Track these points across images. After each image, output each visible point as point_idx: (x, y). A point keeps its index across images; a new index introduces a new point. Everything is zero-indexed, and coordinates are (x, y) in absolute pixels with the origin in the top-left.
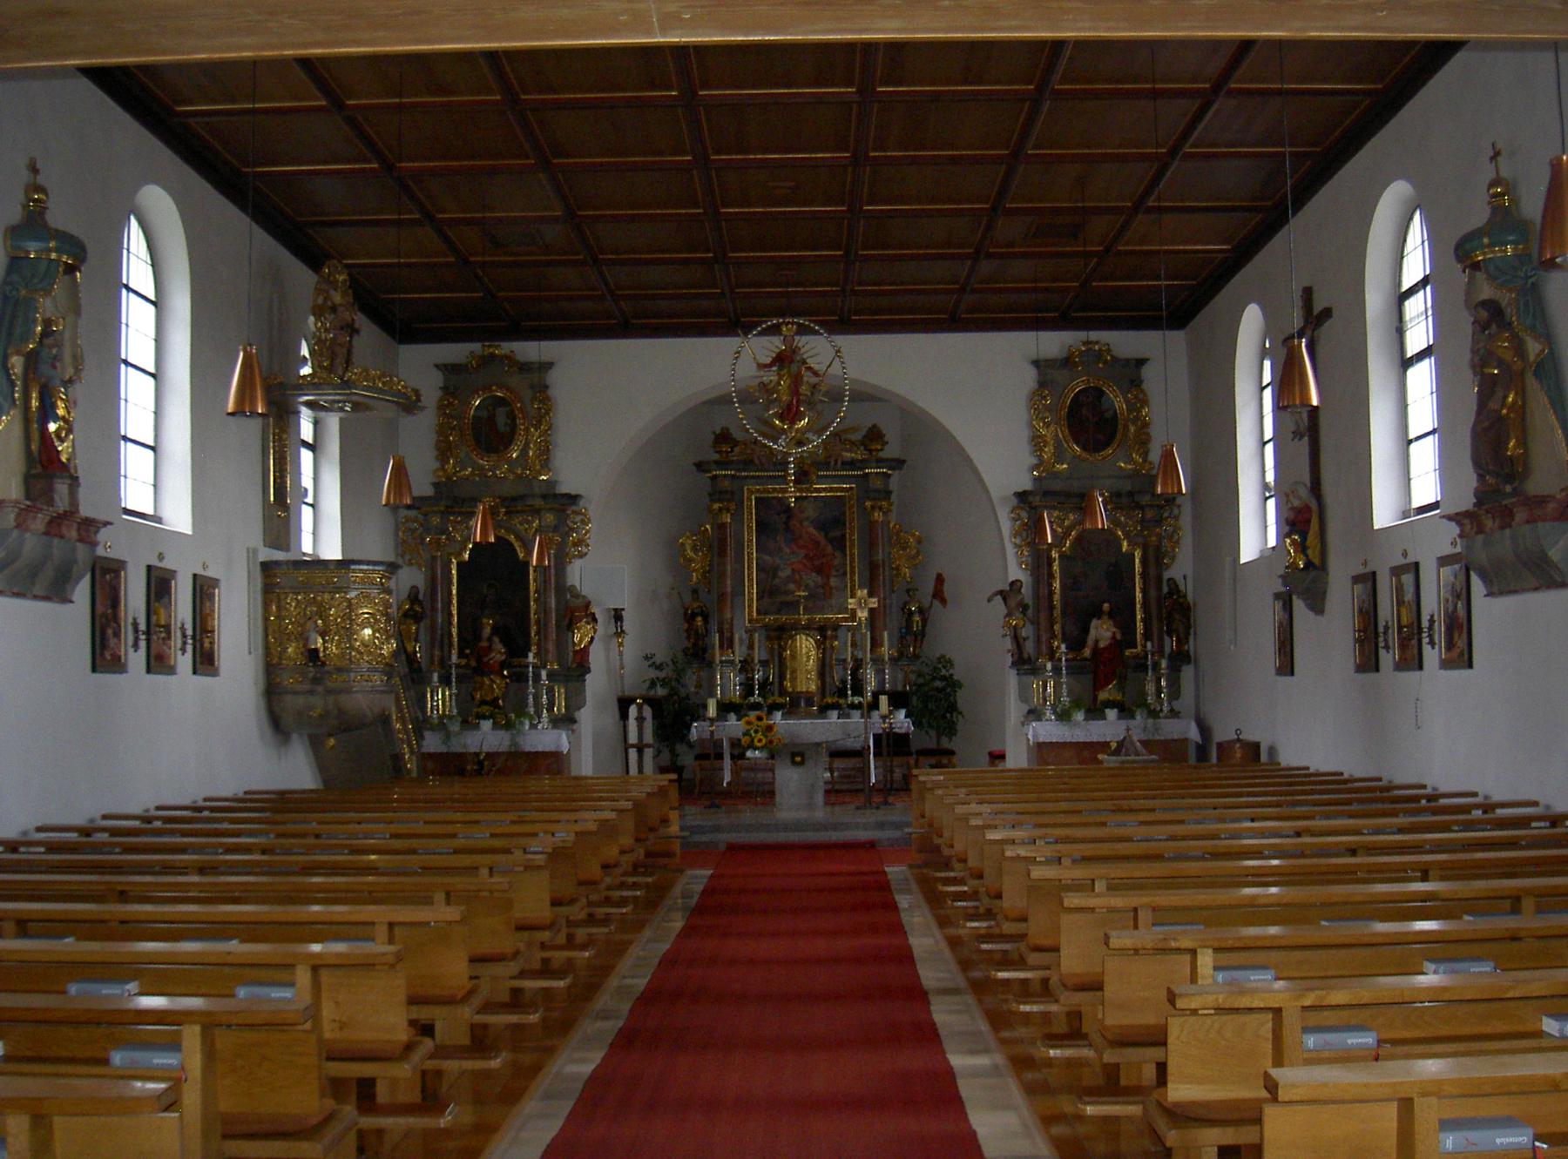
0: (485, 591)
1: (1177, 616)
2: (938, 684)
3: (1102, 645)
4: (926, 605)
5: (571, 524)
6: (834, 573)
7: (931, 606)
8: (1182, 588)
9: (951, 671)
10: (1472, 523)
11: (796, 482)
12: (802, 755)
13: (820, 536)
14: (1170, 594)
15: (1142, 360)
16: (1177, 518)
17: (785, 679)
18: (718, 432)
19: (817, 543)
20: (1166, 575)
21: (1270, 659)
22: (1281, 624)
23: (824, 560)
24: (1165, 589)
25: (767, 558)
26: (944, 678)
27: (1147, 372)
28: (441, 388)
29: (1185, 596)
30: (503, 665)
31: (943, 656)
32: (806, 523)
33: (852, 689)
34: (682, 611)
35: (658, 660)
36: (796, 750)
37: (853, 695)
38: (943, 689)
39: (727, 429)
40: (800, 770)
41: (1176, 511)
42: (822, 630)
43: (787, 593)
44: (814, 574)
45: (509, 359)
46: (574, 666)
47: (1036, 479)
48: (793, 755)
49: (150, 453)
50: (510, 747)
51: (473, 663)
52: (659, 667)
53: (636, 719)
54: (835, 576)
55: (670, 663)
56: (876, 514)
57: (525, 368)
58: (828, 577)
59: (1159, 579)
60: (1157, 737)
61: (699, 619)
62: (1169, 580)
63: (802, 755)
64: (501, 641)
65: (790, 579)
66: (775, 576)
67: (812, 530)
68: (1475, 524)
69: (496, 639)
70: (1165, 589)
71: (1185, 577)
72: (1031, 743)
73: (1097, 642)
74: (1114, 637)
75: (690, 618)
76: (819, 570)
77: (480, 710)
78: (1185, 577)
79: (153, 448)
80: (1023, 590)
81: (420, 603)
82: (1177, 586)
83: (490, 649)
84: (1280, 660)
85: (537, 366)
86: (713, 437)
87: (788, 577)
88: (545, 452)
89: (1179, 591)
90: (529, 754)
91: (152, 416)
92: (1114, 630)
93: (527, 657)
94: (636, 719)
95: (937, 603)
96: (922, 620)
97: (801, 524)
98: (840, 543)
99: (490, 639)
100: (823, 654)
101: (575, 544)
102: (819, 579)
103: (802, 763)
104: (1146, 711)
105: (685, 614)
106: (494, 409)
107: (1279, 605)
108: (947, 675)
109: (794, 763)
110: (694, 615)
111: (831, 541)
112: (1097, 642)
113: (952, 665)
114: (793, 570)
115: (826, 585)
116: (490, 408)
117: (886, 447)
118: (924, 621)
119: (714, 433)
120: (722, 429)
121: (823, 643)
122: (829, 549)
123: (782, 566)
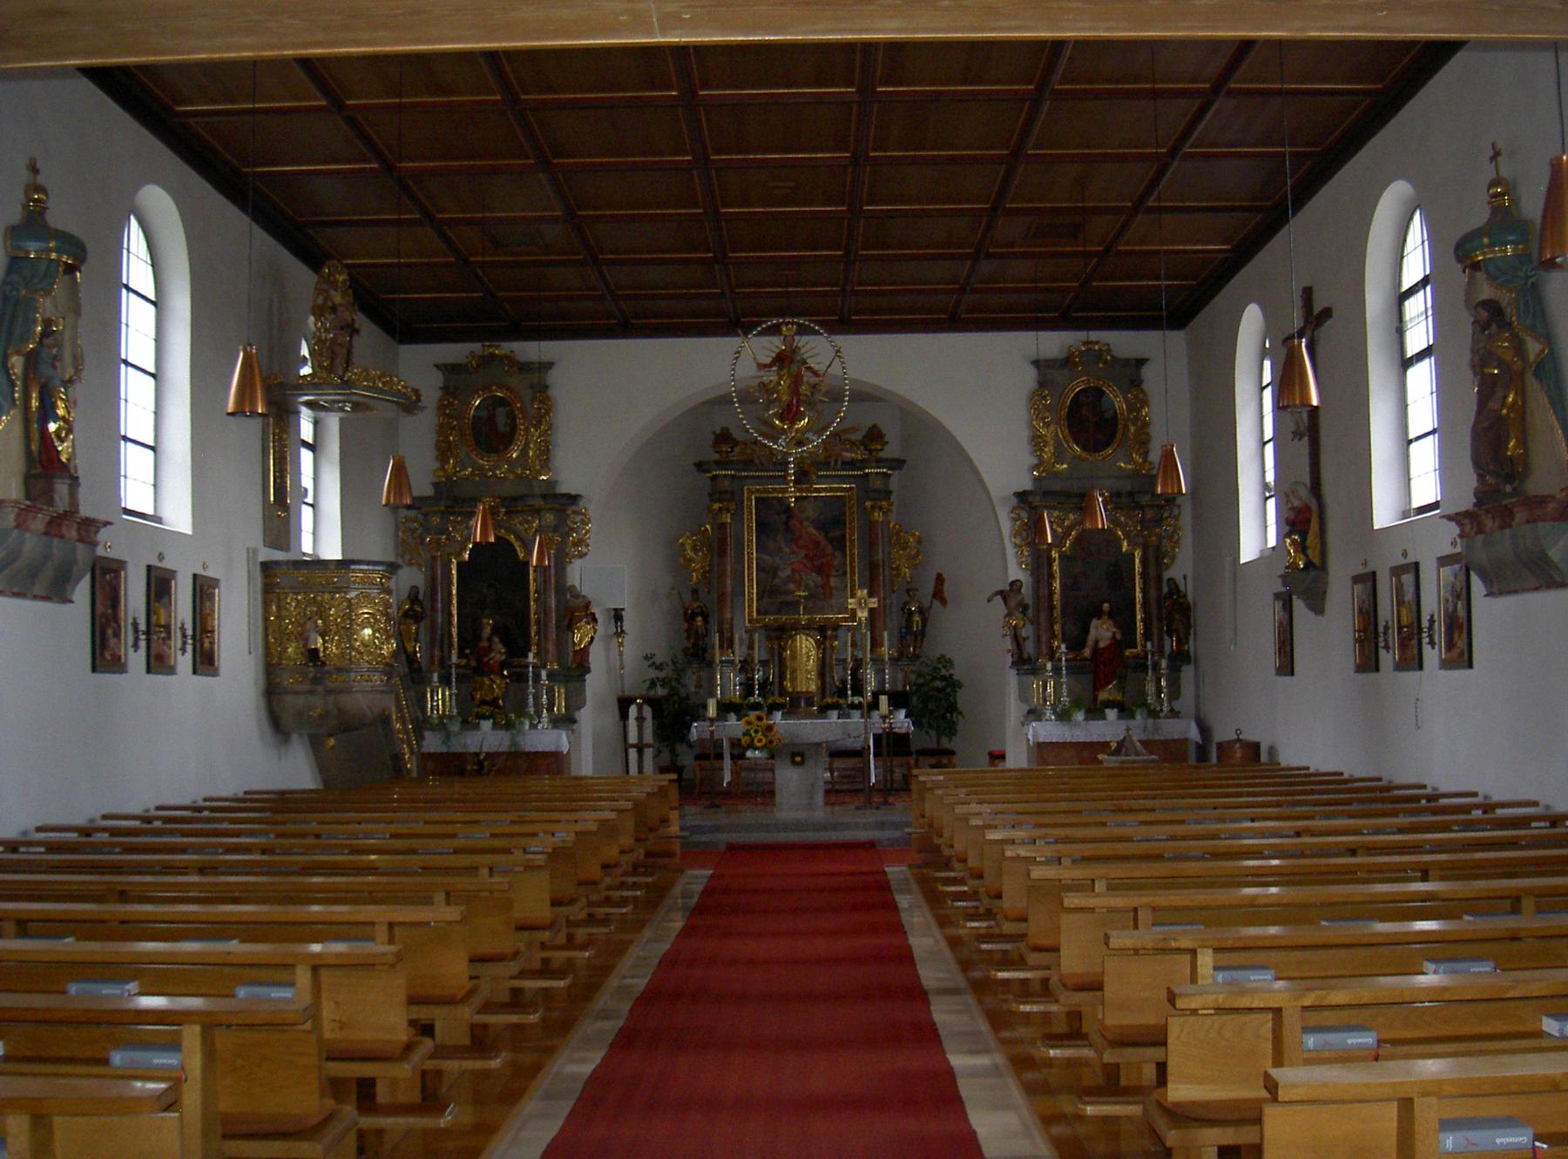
0: (485, 591)
1: (1177, 616)
2: (938, 684)
3: (1102, 645)
4: (926, 605)
5: (571, 524)
6: (834, 573)
7: (931, 606)
8: (1182, 588)
9: (951, 671)
10: (1472, 523)
11: (796, 482)
12: (802, 755)
13: (820, 536)
14: (1170, 594)
15: (1142, 360)
16: (1177, 518)
17: (785, 679)
18: (718, 432)
19: (817, 543)
20: (1166, 575)
21: (1270, 659)
22: (1281, 624)
23: (824, 560)
24: (1165, 589)
25: (767, 558)
26: (944, 678)
27: (1147, 372)
28: (441, 388)
29: (1185, 596)
30: (503, 665)
31: (943, 656)
32: (806, 523)
33: (852, 689)
34: (682, 611)
35: (658, 660)
36: (796, 750)
37: (853, 695)
38: (943, 689)
39: (727, 429)
40: (800, 770)
41: (1176, 511)
42: (822, 630)
43: (787, 593)
44: (814, 574)
45: (509, 359)
46: (574, 666)
47: (1036, 479)
48: (793, 755)
49: (150, 453)
50: (510, 747)
51: (473, 663)
52: (659, 667)
53: (636, 719)
54: (835, 576)
55: (670, 663)
56: (876, 514)
57: (525, 368)
58: (828, 577)
59: (1159, 579)
60: (1157, 737)
61: (699, 619)
62: (1169, 580)
63: (802, 755)
64: (501, 641)
65: (790, 579)
66: (775, 576)
67: (812, 530)
68: (1475, 524)
69: (496, 639)
70: (1165, 589)
71: (1185, 577)
72: (1031, 743)
73: (1097, 642)
74: (1114, 637)
75: (690, 618)
76: (819, 570)
77: (480, 710)
78: (1185, 577)
79: (153, 448)
80: (1023, 590)
81: (420, 603)
82: (1177, 586)
83: (490, 649)
84: (1280, 660)
85: (537, 366)
86: (713, 437)
87: (788, 577)
88: (545, 452)
89: (1179, 591)
90: (529, 754)
91: (152, 416)
92: (1114, 630)
93: (527, 657)
94: (636, 719)
95: (937, 603)
96: (922, 620)
97: (801, 524)
98: (840, 543)
99: (490, 639)
100: (823, 654)
101: (575, 544)
102: (819, 579)
103: (802, 763)
104: (1146, 711)
105: (685, 614)
106: (494, 409)
107: (1279, 605)
108: (947, 675)
109: (794, 763)
110: (694, 615)
111: (831, 541)
112: (1097, 642)
113: (952, 665)
114: (793, 570)
115: (826, 585)
116: (490, 408)
117: (886, 447)
118: (924, 621)
119: (714, 433)
120: (722, 429)
121: (823, 643)
122: (829, 549)
123: (782, 566)
